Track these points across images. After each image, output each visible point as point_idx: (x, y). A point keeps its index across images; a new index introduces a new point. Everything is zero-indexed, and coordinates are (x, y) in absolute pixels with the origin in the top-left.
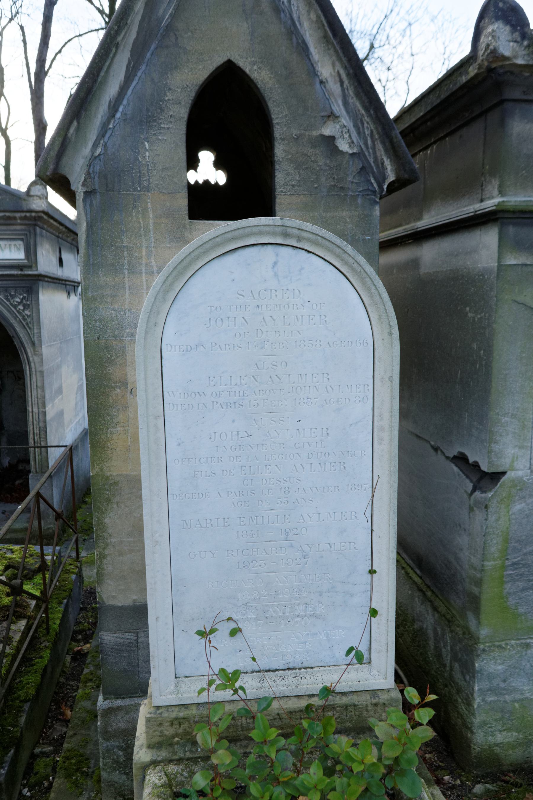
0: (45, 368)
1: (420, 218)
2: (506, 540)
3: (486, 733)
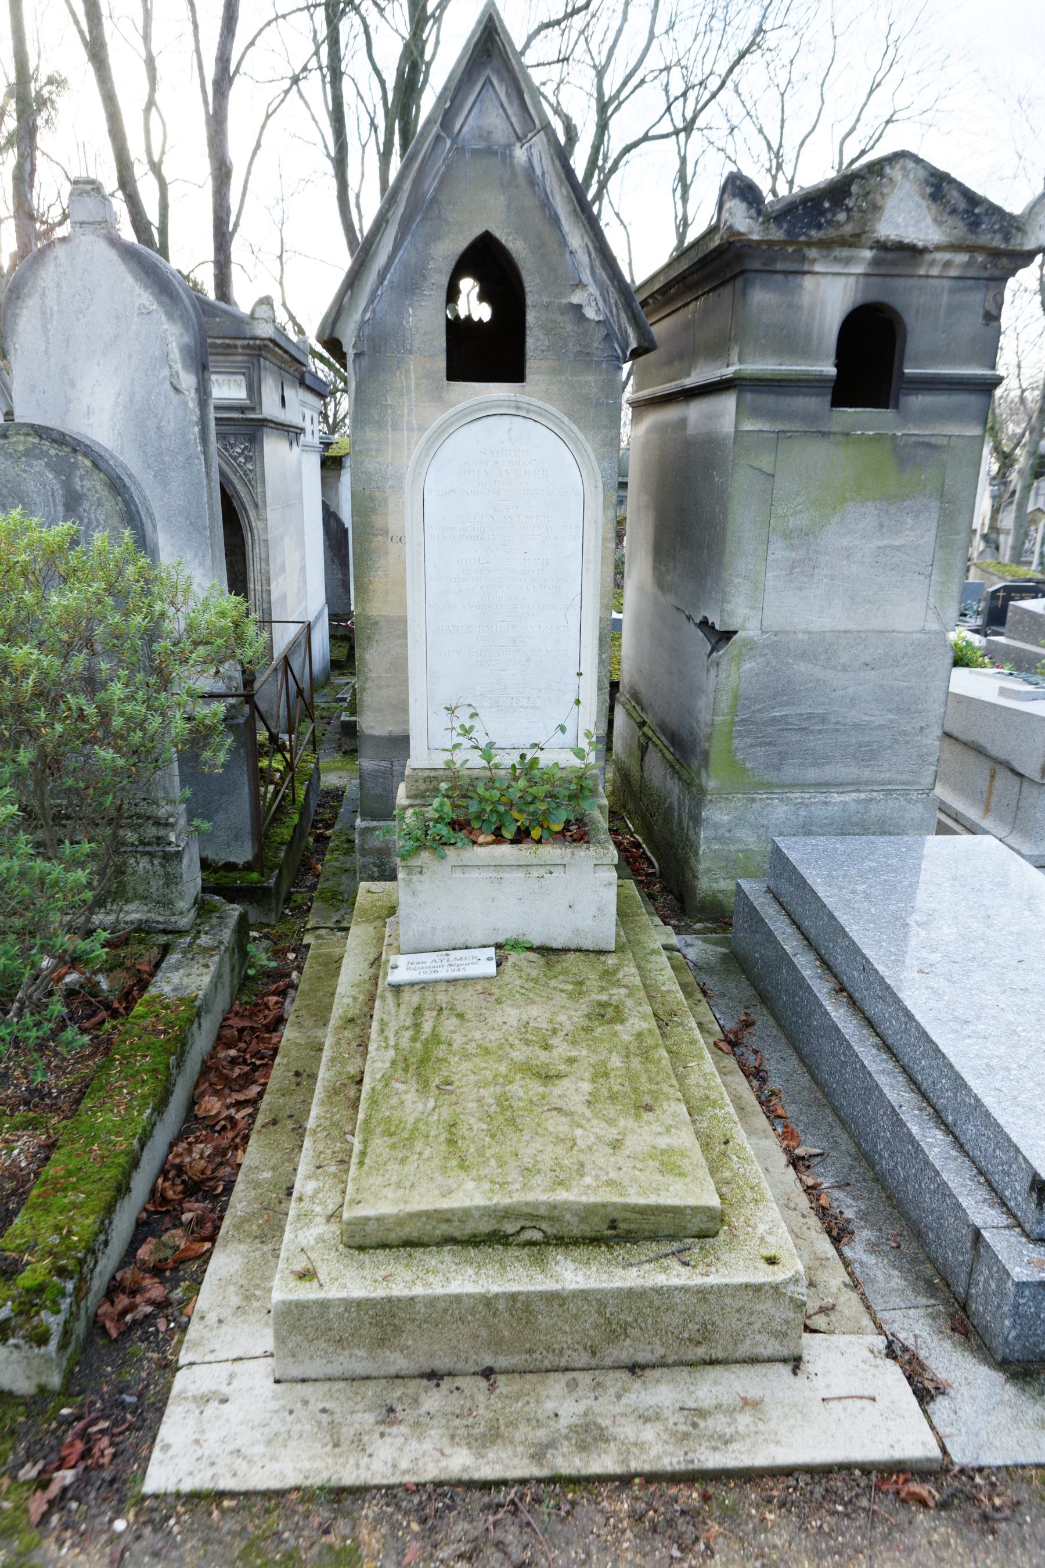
0: (270, 536)
1: (688, 375)
2: (736, 697)
3: (711, 880)
